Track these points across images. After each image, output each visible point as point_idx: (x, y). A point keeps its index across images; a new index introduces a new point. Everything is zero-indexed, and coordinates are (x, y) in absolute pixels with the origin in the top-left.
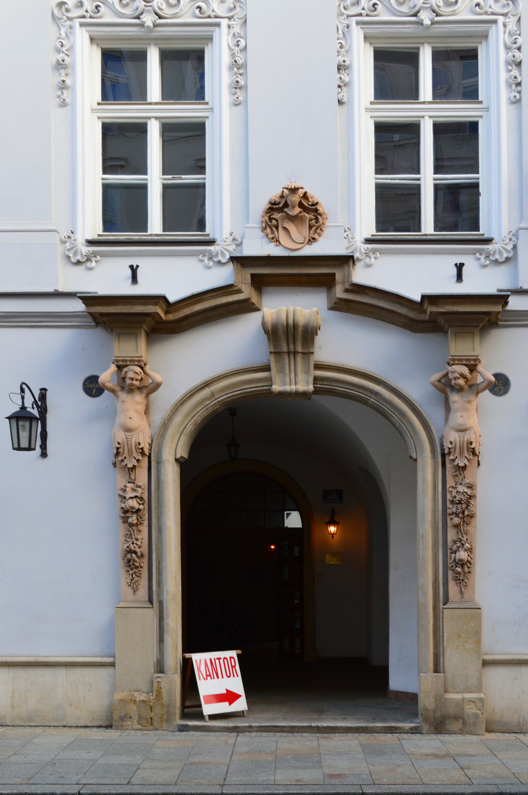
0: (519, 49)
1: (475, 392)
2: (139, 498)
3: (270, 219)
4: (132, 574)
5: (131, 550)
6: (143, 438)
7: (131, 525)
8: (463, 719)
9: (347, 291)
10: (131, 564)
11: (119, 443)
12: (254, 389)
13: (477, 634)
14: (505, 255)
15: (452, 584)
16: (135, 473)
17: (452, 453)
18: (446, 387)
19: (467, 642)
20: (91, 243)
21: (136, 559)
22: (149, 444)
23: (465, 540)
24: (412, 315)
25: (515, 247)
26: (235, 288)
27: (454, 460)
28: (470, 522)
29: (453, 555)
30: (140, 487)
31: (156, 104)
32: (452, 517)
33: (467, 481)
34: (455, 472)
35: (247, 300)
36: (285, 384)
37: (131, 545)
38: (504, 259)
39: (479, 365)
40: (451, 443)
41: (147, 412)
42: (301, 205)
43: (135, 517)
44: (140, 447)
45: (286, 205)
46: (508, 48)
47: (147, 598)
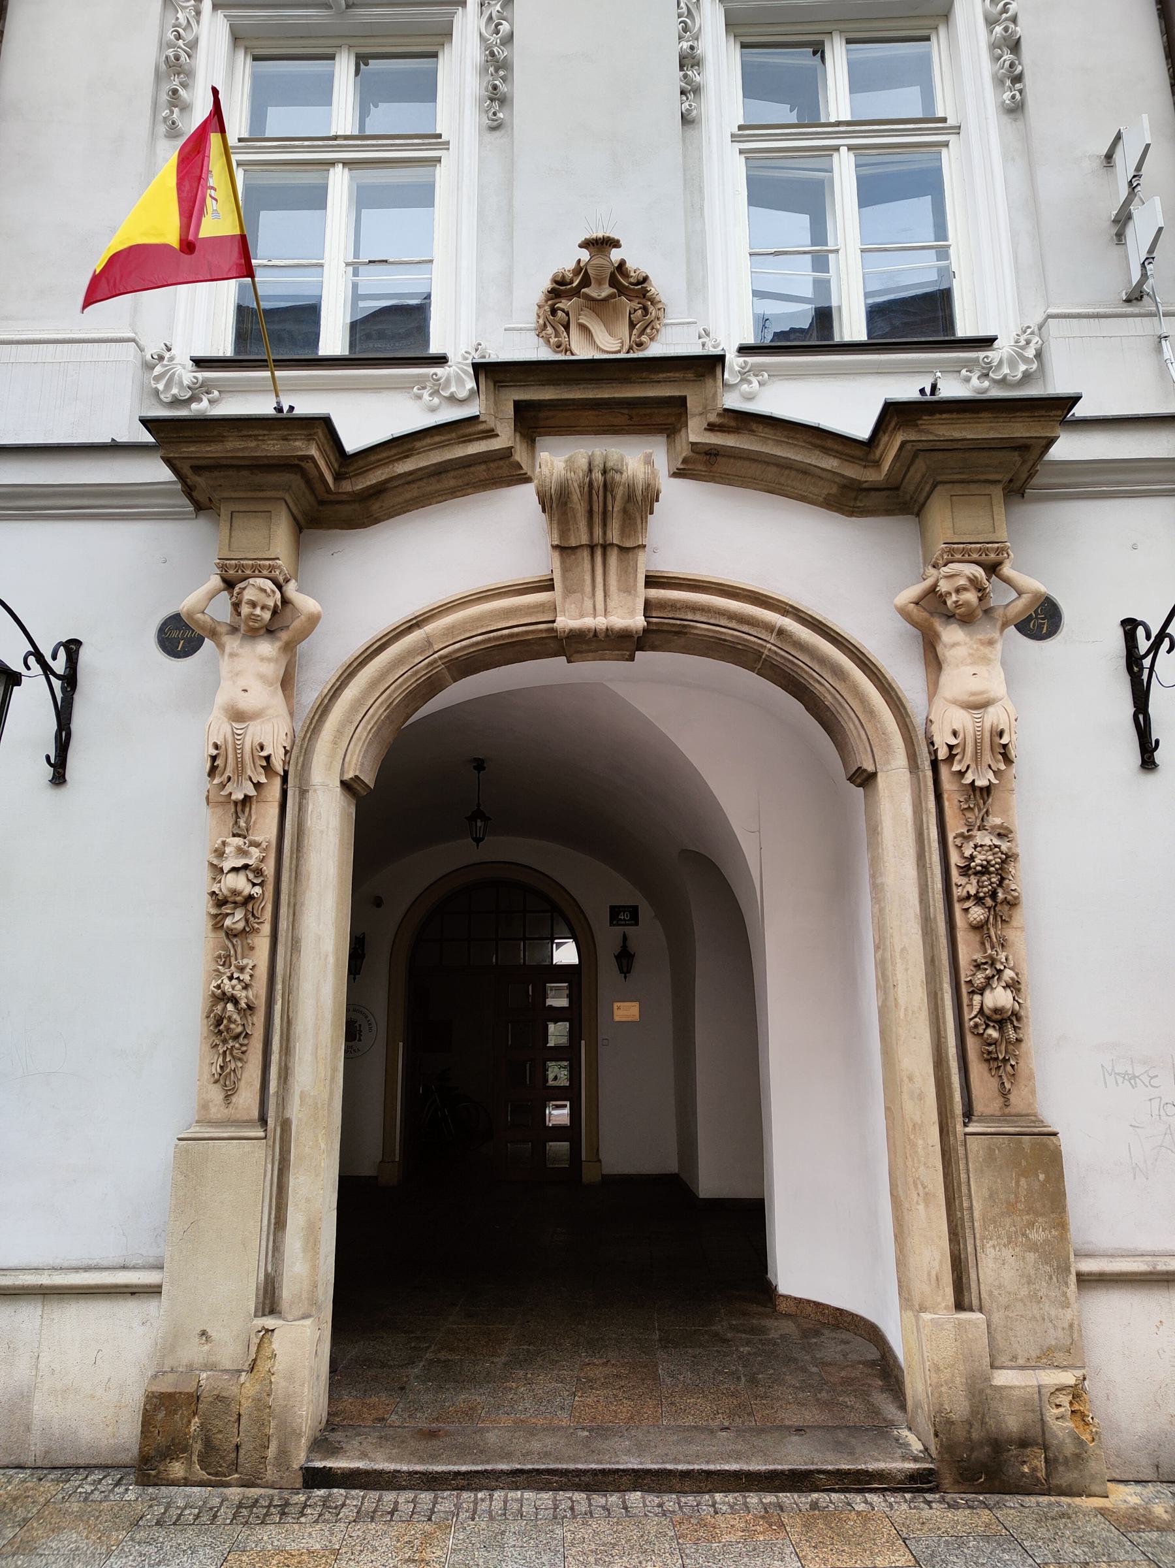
0: (1014, 19)
1: (999, 623)
2: (254, 871)
3: (554, 311)
4: (225, 1052)
5: (224, 993)
6: (272, 733)
7: (231, 934)
8: (1046, 1448)
9: (711, 428)
10: (222, 1027)
11: (216, 747)
12: (516, 630)
13: (1053, 1200)
14: (1023, 367)
15: (977, 1069)
16: (250, 814)
17: (958, 758)
18: (932, 614)
19: (1031, 1225)
20: (201, 363)
21: (235, 1016)
22: (286, 752)
23: (1003, 960)
24: (852, 472)
25: (1039, 355)
26: (482, 427)
27: (961, 774)
28: (1010, 917)
29: (977, 998)
30: (257, 845)
31: (346, 138)
32: (966, 905)
33: (995, 820)
34: (967, 801)
35: (507, 453)
36: (582, 616)
37: (226, 981)
38: (1020, 375)
39: (1007, 561)
40: (955, 734)
41: (287, 683)
42: (613, 282)
43: (239, 914)
44: (264, 754)
45: (586, 282)
46: (991, 22)
47: (255, 1114)
